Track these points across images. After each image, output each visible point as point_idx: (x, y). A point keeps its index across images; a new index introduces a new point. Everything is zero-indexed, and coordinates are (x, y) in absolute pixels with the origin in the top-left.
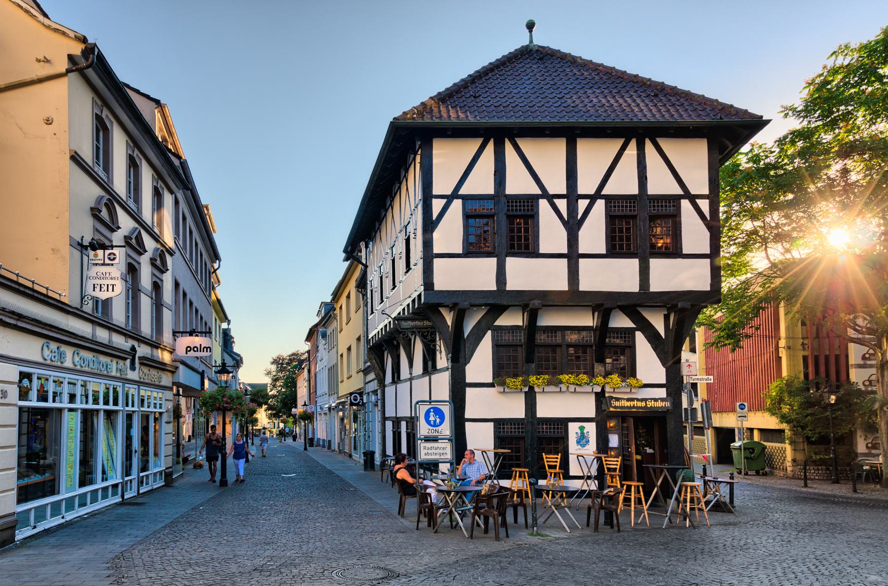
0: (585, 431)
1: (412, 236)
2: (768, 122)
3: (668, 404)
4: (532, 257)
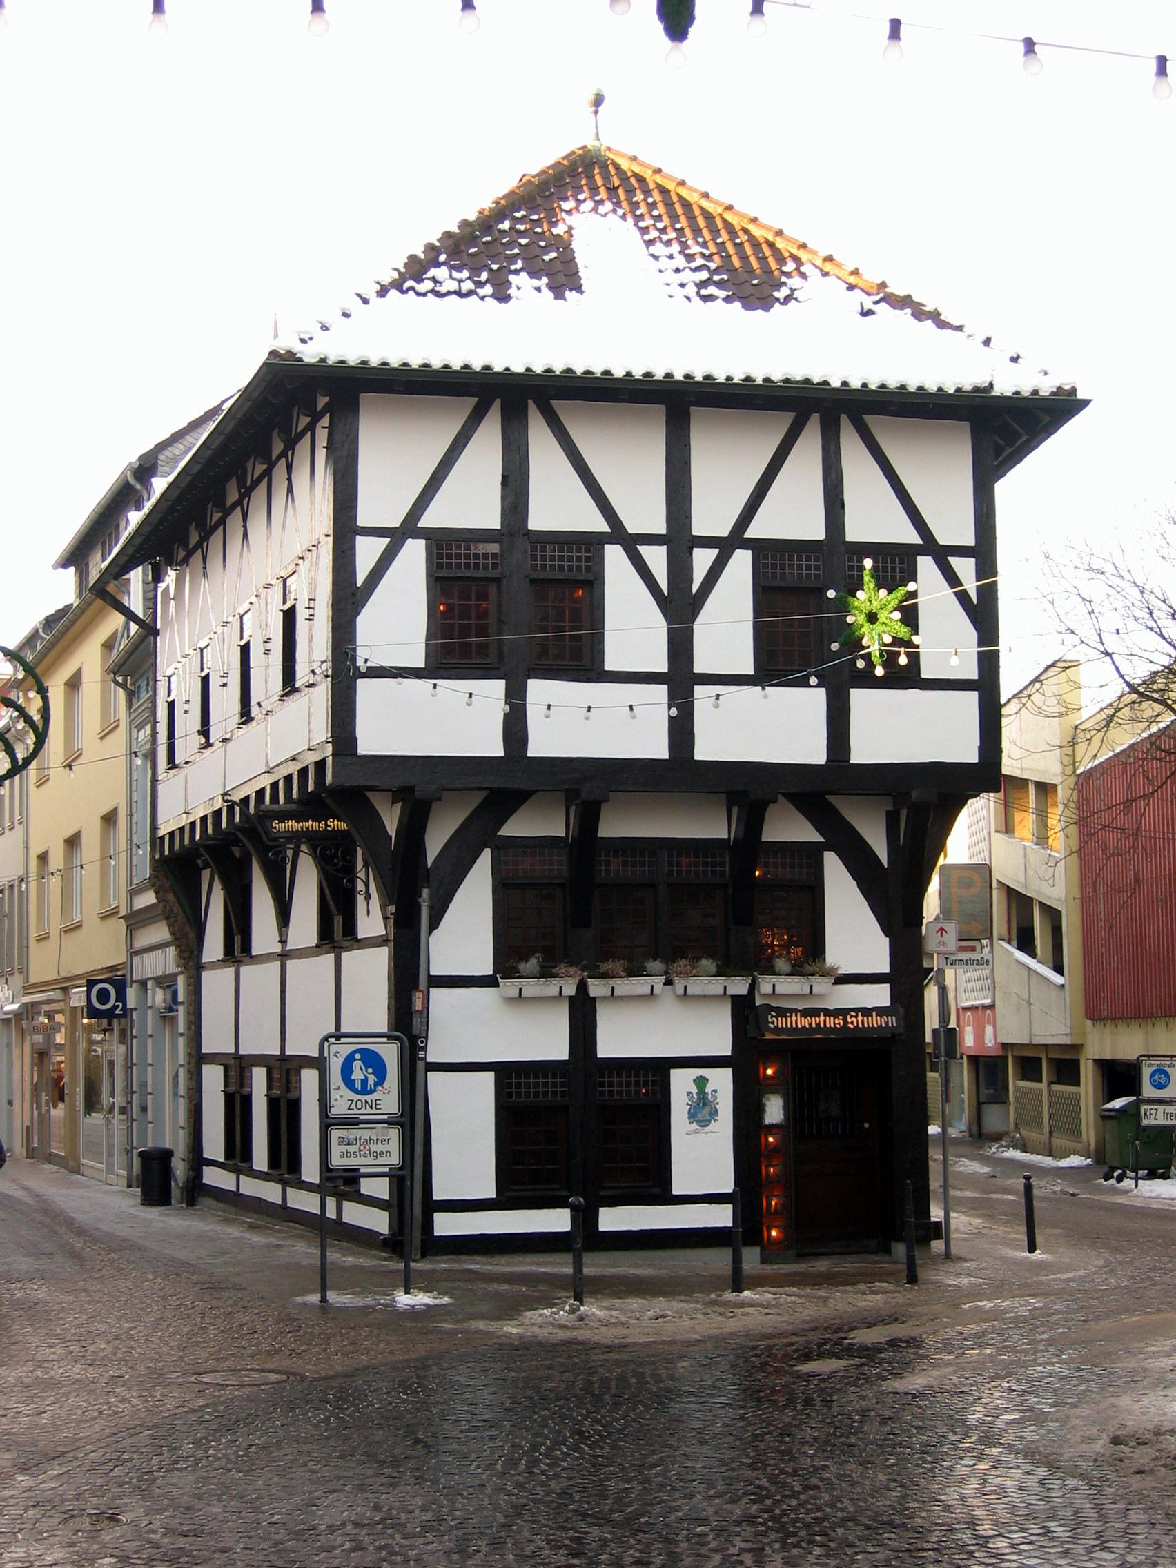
0: (708, 1089)
1: (302, 614)
2: (1086, 403)
3: (892, 1021)
4: (588, 681)
